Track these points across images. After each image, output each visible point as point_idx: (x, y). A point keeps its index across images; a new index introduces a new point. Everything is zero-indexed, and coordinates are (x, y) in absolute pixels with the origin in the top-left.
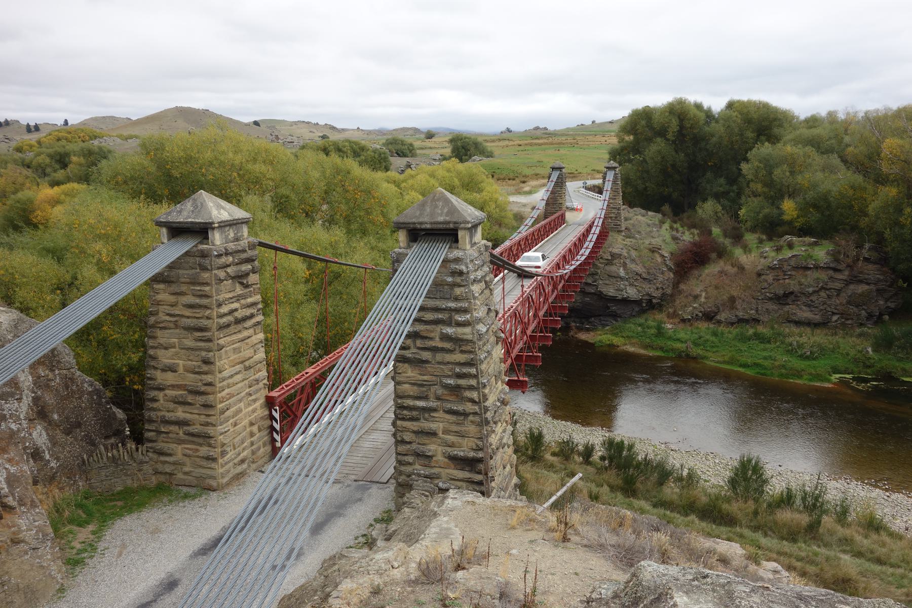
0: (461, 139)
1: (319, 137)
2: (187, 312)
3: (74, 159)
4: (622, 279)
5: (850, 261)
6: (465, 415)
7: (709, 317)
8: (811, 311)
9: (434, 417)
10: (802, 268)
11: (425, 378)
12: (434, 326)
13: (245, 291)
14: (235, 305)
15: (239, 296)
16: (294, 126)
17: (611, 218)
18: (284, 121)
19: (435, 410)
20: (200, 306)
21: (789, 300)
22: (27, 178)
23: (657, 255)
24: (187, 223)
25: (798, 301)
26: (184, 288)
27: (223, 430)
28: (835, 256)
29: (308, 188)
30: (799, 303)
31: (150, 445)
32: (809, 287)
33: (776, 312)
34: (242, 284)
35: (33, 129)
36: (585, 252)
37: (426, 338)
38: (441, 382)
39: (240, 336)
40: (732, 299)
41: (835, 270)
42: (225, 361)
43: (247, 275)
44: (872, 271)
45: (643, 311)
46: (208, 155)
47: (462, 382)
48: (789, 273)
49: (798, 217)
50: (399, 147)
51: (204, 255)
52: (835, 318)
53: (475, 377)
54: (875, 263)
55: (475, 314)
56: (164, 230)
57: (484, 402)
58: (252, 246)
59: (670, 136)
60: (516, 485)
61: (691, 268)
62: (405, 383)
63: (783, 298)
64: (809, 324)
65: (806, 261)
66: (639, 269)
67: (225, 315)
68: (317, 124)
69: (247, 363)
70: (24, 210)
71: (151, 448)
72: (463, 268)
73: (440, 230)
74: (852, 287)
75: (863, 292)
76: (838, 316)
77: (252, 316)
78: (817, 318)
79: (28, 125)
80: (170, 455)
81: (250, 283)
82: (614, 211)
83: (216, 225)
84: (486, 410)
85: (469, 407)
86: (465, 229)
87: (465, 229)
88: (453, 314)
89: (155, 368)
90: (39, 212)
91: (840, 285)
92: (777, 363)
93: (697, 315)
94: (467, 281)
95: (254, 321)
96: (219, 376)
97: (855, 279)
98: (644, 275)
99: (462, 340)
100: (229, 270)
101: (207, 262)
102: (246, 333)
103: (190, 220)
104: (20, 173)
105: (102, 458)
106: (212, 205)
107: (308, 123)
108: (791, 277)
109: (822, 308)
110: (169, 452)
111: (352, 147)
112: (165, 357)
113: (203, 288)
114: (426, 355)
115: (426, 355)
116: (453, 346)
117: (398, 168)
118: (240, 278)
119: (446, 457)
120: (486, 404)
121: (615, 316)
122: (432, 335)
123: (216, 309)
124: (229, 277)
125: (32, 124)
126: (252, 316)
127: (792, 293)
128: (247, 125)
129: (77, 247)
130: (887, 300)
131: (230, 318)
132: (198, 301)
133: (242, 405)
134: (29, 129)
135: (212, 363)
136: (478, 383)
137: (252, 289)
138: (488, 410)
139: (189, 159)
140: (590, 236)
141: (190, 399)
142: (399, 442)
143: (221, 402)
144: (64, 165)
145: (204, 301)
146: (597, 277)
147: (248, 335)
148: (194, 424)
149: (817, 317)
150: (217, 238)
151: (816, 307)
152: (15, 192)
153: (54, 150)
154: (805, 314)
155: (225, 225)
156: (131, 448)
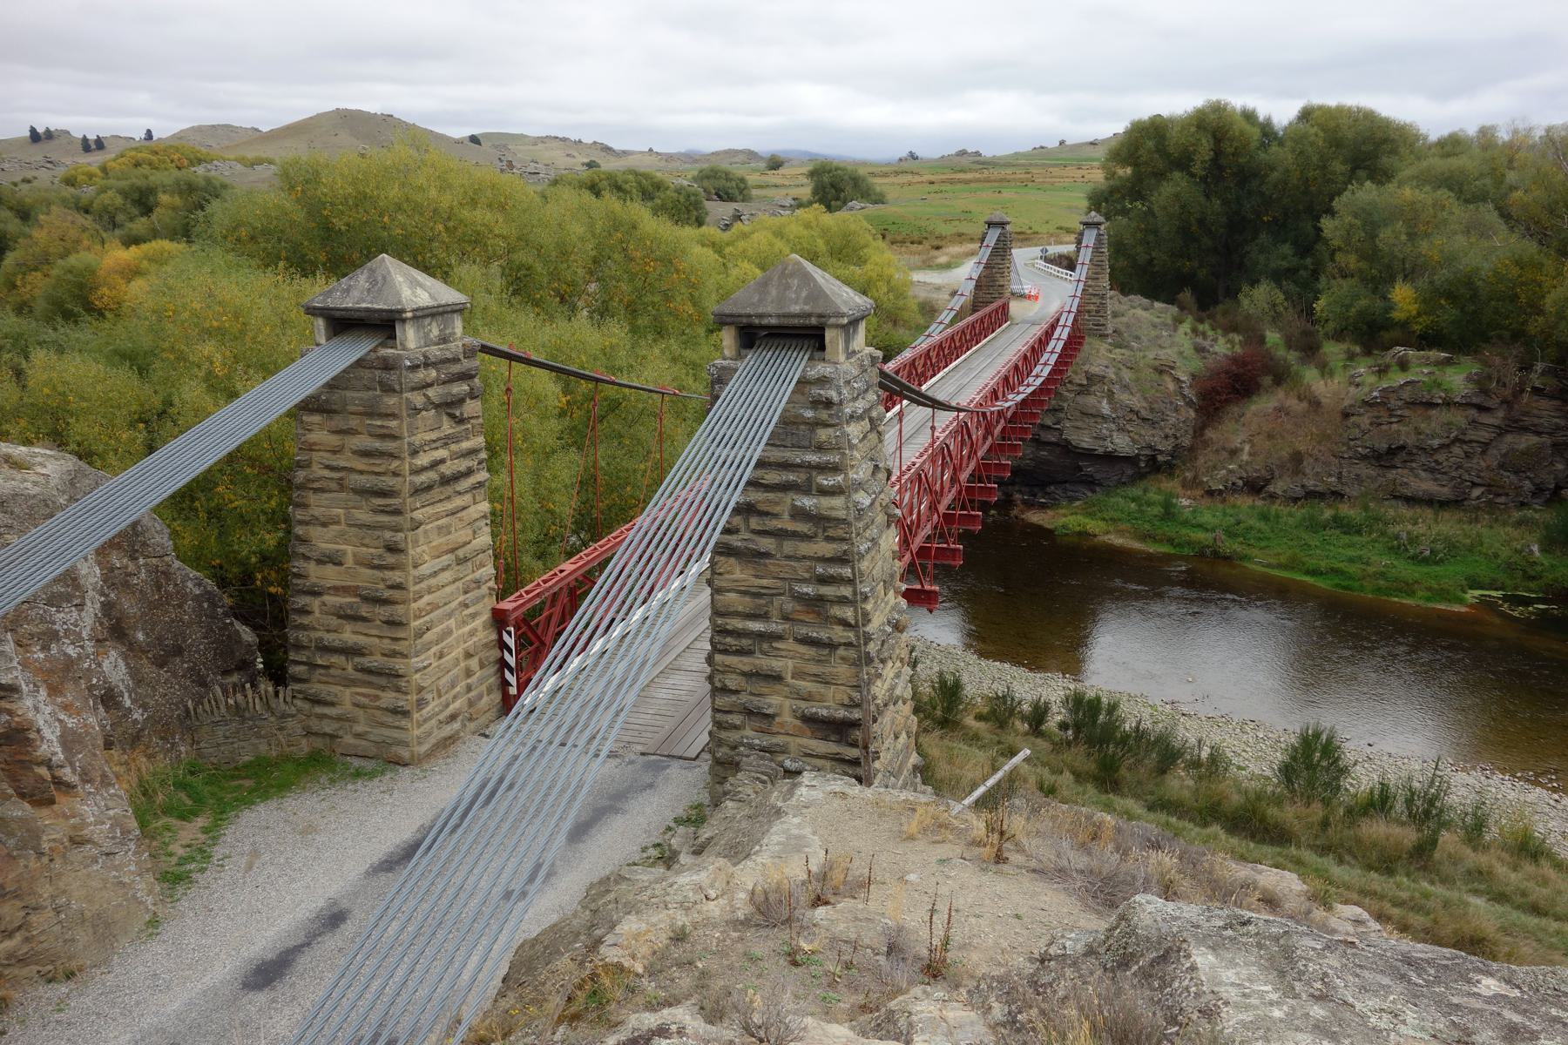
1: (583, 164)
2: (360, 464)
3: (164, 198)
6: (832, 646)
7: (1255, 487)
8: (1436, 480)
9: (778, 649)
11: (764, 582)
12: (780, 495)
13: (458, 429)
14: (442, 453)
15: (447, 437)
17: (1089, 312)
18: (522, 136)
21: (1397, 461)
22: (84, 231)
23: (1168, 379)
24: (359, 310)
25: (1412, 461)
26: (354, 422)
27: (421, 665)
28: (1481, 384)
29: (564, 253)
30: (1414, 465)
35: (93, 147)
36: (1042, 371)
37: (767, 514)
38: (791, 589)
39: (449, 506)
41: (1481, 408)
43: (461, 401)
46: (394, 192)
47: (827, 591)
48: (1399, 412)
50: (722, 183)
51: (388, 365)
52: (1476, 492)
53: (850, 582)
54: (1552, 397)
58: (470, 352)
59: (1197, 169)
60: (915, 767)
61: (1227, 401)
62: (729, 591)
63: (1387, 457)
64: (1430, 501)
65: (1429, 391)
66: (1136, 402)
67: (424, 469)
68: (580, 141)
71: (300, 692)
72: (833, 394)
74: (1509, 438)
75: (1528, 448)
76: (1482, 489)
77: (469, 472)
78: (1446, 492)
79: (85, 139)
80: (332, 704)
81: (465, 416)
84: (868, 638)
85: (839, 634)
86: (837, 326)
87: (837, 326)
88: (814, 474)
90: (105, 290)
92: (1371, 570)
93: (1234, 484)
94: (839, 418)
95: (472, 480)
97: (1515, 425)
98: (1144, 413)
99: (828, 519)
100: (431, 392)
101: (392, 377)
102: (458, 502)
103: (364, 305)
104: (73, 222)
105: (218, 708)
106: (401, 279)
107: (564, 140)
108: (1401, 419)
109: (1454, 474)
111: (639, 183)
112: (322, 540)
114: (766, 544)
115: (766, 544)
118: (449, 406)
119: (797, 718)
120: (867, 629)
121: (1091, 483)
122: (777, 509)
123: (408, 459)
125: (92, 137)
126: (469, 472)
127: (1402, 448)
128: (459, 142)
129: (172, 349)
131: (432, 475)
132: (378, 444)
134: (86, 145)
136: (855, 593)
139: (362, 199)
141: (364, 610)
142: (719, 690)
144: (147, 210)
145: (389, 446)
147: (463, 504)
150: (410, 337)
153: (128, 182)
154: (1423, 484)
156: (266, 691)
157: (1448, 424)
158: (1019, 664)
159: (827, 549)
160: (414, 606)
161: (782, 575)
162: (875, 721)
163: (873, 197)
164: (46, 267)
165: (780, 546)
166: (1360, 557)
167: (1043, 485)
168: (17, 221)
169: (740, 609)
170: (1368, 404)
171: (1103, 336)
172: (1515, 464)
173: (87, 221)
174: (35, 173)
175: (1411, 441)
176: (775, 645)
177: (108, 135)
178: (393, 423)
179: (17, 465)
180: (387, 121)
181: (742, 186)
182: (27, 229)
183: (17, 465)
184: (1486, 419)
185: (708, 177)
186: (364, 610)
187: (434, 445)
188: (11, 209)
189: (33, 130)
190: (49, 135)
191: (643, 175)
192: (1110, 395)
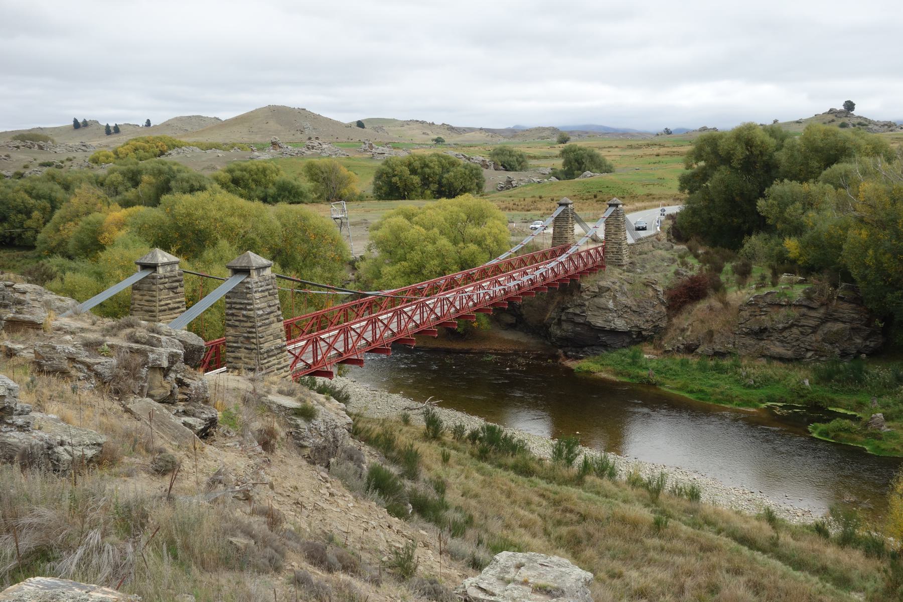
0: (575, 151)
1: (433, 140)
2: (146, 304)
3: (145, 178)
4: (610, 310)
5: (824, 299)
6: (252, 349)
7: (690, 349)
8: (784, 347)
10: (775, 304)
16: (406, 126)
17: (613, 252)
18: (394, 120)
21: (764, 336)
22: (98, 198)
23: (650, 290)
25: (771, 336)
26: (145, 293)
28: (808, 296)
29: (272, 235)
30: (772, 338)
32: (779, 323)
33: (754, 346)
35: (113, 131)
39: (171, 316)
40: (711, 333)
41: (810, 308)
43: (177, 288)
44: (846, 310)
45: (635, 342)
46: (200, 212)
47: (250, 335)
48: (765, 309)
49: (801, 255)
50: (507, 158)
51: (154, 278)
52: (809, 354)
53: (255, 333)
54: (850, 302)
56: (139, 267)
58: (180, 275)
59: (735, 164)
61: (685, 302)
63: (761, 333)
64: (781, 359)
65: (779, 298)
66: (629, 302)
68: (433, 124)
70: (94, 232)
72: (250, 286)
74: (829, 324)
75: (838, 330)
76: (812, 353)
77: (179, 308)
78: (789, 354)
79: (108, 126)
85: (253, 346)
90: (107, 234)
91: (813, 323)
92: (718, 390)
93: (678, 347)
97: (829, 318)
98: (634, 308)
100: (166, 285)
101: (154, 281)
102: (175, 315)
104: (93, 193)
107: (423, 122)
108: (766, 313)
109: (794, 344)
111: (440, 162)
114: (237, 323)
115: (237, 323)
117: (497, 184)
118: (172, 289)
121: (605, 346)
124: (165, 288)
125: (112, 124)
126: (179, 308)
127: (766, 329)
128: (349, 126)
129: (109, 272)
130: (865, 339)
131: (166, 307)
132: (151, 298)
134: (108, 131)
139: (189, 215)
144: (136, 183)
145: (153, 299)
146: (585, 308)
149: (790, 353)
150: (161, 270)
151: (788, 343)
152: (88, 213)
153: (126, 167)
154: (777, 349)
157: (787, 316)
158: (462, 411)
159: (249, 324)
163: (604, 168)
164: (77, 219)
166: (716, 385)
167: (582, 347)
168: (63, 191)
170: (749, 304)
171: (620, 266)
172: (830, 339)
173: (100, 192)
174: (74, 154)
175: (768, 324)
177: (122, 123)
179: (62, 301)
180: (302, 113)
181: (521, 159)
182: (68, 196)
183: (62, 301)
184: (813, 314)
185: (497, 154)
188: (59, 183)
189: (76, 121)
190: (86, 124)
191: (443, 157)
192: (615, 297)
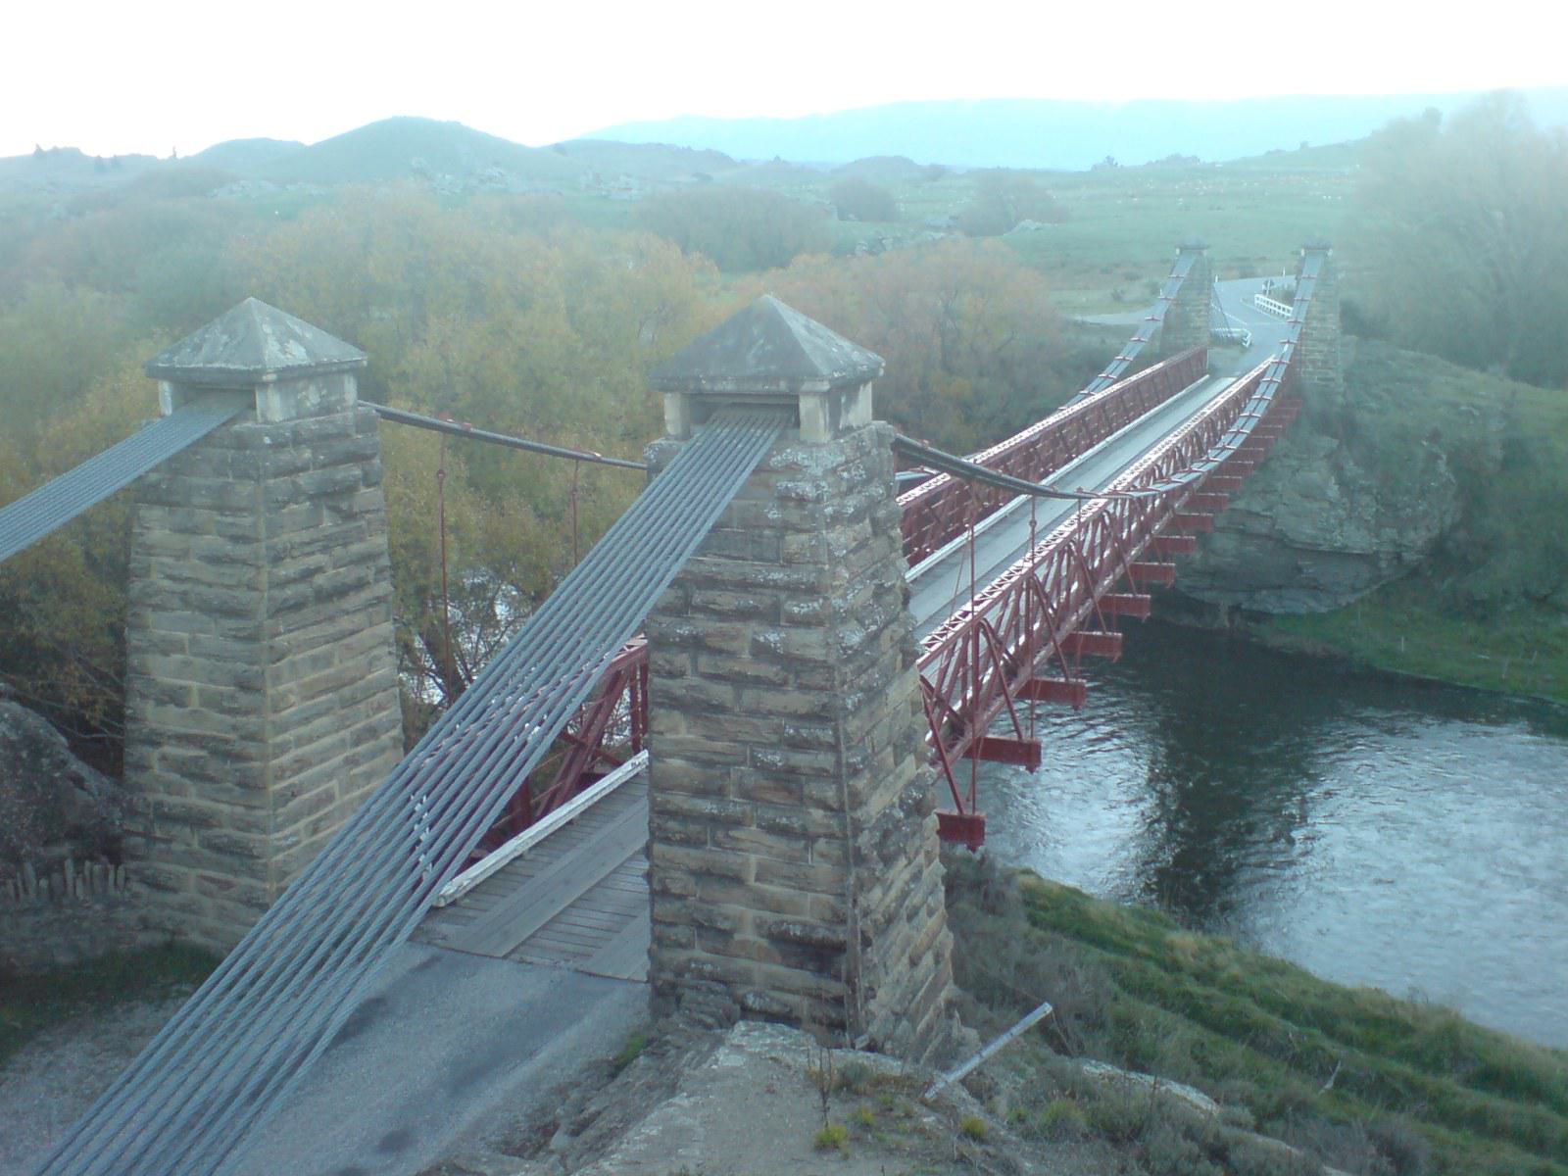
2: (208, 573)
9: (737, 839)
11: (719, 745)
12: (739, 625)
13: (345, 527)
14: (313, 561)
15: (328, 538)
19: (738, 823)
20: (233, 561)
24: (210, 371)
27: (283, 843)
31: (133, 865)
34: (336, 510)
36: (1231, 443)
37: (720, 651)
38: (753, 757)
42: (292, 685)
43: (350, 489)
47: (800, 759)
55: (837, 602)
56: (165, 387)
57: (853, 809)
60: (950, 1004)
62: (671, 756)
67: (289, 581)
69: (347, 691)
71: (136, 872)
73: (759, 395)
80: (174, 891)
81: (356, 509)
82: (1321, 347)
83: (272, 377)
84: (858, 828)
86: (815, 394)
87: (815, 394)
88: (783, 596)
89: (144, 696)
94: (814, 520)
95: (365, 595)
96: (272, 717)
99: (804, 661)
100: (303, 479)
102: (345, 623)
103: (217, 365)
105: (26, 890)
106: (267, 329)
110: (170, 883)
112: (163, 670)
113: (238, 520)
114: (722, 692)
115: (722, 692)
116: (783, 674)
119: (763, 936)
120: (859, 814)
122: (734, 645)
123: (268, 568)
126: (361, 585)
132: (229, 548)
133: (334, 783)
135: (258, 690)
136: (838, 763)
137: (363, 523)
138: (862, 830)
140: (1251, 405)
141: (214, 767)
142: (660, 894)
143: (279, 778)
145: (242, 551)
147: (351, 627)
148: (220, 826)
150: (273, 407)
155: (289, 378)
156: (91, 872)
160: (275, 762)
161: (741, 737)
162: (867, 942)
165: (738, 697)
169: (686, 781)
176: (732, 833)
178: (247, 520)
186: (214, 767)
187: (308, 549)
